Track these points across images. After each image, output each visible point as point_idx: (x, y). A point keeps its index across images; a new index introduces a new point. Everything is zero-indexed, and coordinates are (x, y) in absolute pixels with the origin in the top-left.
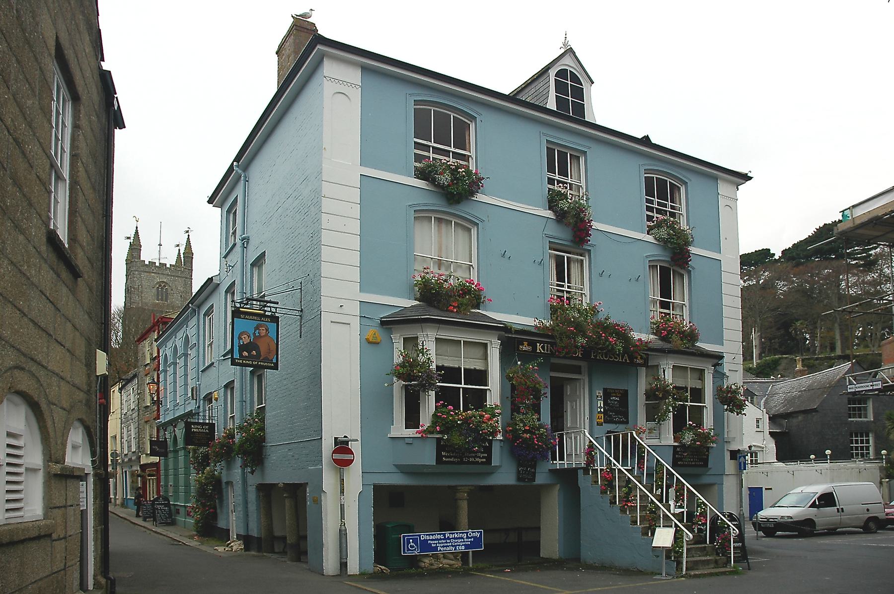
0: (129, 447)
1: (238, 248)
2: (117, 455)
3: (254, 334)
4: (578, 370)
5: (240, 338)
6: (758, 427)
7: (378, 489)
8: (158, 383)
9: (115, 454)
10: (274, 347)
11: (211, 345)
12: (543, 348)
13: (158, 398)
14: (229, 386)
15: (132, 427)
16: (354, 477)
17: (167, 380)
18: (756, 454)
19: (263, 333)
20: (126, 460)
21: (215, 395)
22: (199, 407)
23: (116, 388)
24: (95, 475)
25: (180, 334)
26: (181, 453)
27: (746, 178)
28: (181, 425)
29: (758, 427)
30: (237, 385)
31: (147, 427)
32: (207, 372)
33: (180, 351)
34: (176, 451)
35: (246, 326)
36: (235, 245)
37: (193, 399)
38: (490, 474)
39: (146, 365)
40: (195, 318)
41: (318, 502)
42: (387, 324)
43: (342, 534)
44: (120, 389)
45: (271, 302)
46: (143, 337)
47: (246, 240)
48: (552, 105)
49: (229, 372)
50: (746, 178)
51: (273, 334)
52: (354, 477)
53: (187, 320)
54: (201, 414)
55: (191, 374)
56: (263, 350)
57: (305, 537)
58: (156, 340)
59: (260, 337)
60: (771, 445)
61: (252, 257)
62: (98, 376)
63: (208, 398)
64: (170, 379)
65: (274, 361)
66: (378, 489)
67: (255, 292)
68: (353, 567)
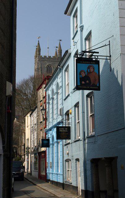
0: (34, 144)
1: (79, 33)
2: (29, 148)
3: (87, 71)
5: (80, 74)
8: (45, 110)
9: (28, 148)
10: (97, 78)
11: (68, 84)
13: (46, 117)
14: (77, 105)
15: (35, 133)
17: (49, 108)
19: (92, 70)
20: (33, 150)
21: (70, 111)
22: (63, 119)
23: (29, 115)
24: (4, 156)
25: (55, 83)
26: (56, 145)
28: (55, 129)
30: (80, 104)
31: (42, 132)
32: (67, 100)
33: (55, 91)
34: (53, 144)
35: (84, 67)
36: (77, 32)
37: (61, 115)
39: (41, 101)
40: (61, 73)
44: (31, 115)
46: (40, 88)
47: (82, 28)
49: (78, 96)
51: (96, 71)
53: (58, 75)
54: (64, 122)
55: (60, 102)
56: (92, 79)
58: (45, 88)
59: (90, 72)
61: (84, 36)
62: (7, 96)
63: (67, 114)
64: (51, 106)
65: (98, 85)
67: (87, 47)
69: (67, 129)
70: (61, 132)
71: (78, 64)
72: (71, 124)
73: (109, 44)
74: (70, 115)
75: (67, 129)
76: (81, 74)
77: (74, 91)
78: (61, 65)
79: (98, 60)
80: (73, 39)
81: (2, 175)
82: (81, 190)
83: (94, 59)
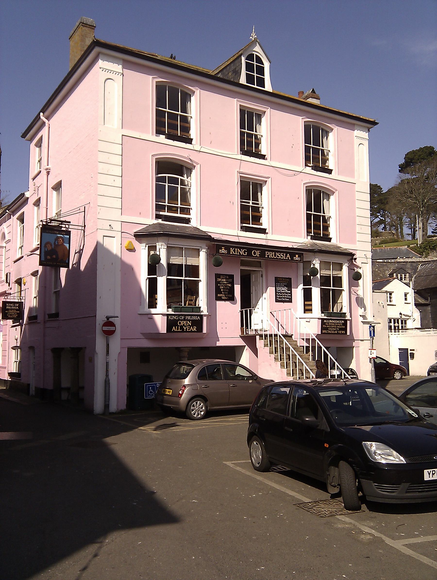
1: (44, 173)
3: (55, 243)
4: (259, 264)
5: (45, 246)
6: (406, 299)
7: (131, 351)
12: (234, 251)
16: (117, 344)
18: (405, 321)
27: (376, 124)
29: (406, 299)
37: (7, 282)
38: (201, 338)
41: (92, 360)
42: (139, 236)
43: (107, 383)
45: (65, 222)
48: (243, 80)
50: (376, 124)
52: (117, 344)
57: (83, 388)
59: (58, 245)
60: (417, 314)
61: (53, 182)
65: (67, 262)
66: (131, 351)
68: (113, 408)
69: (17, 305)
70: (8, 309)
71: (43, 233)
72: (24, 298)
73: (85, 211)
74: (23, 285)
75: (17, 305)
76: (46, 247)
77: (31, 254)
78: (12, 209)
79: (69, 230)
80: (34, 179)
81: (126, 392)
82: (35, 387)
83: (64, 229)
